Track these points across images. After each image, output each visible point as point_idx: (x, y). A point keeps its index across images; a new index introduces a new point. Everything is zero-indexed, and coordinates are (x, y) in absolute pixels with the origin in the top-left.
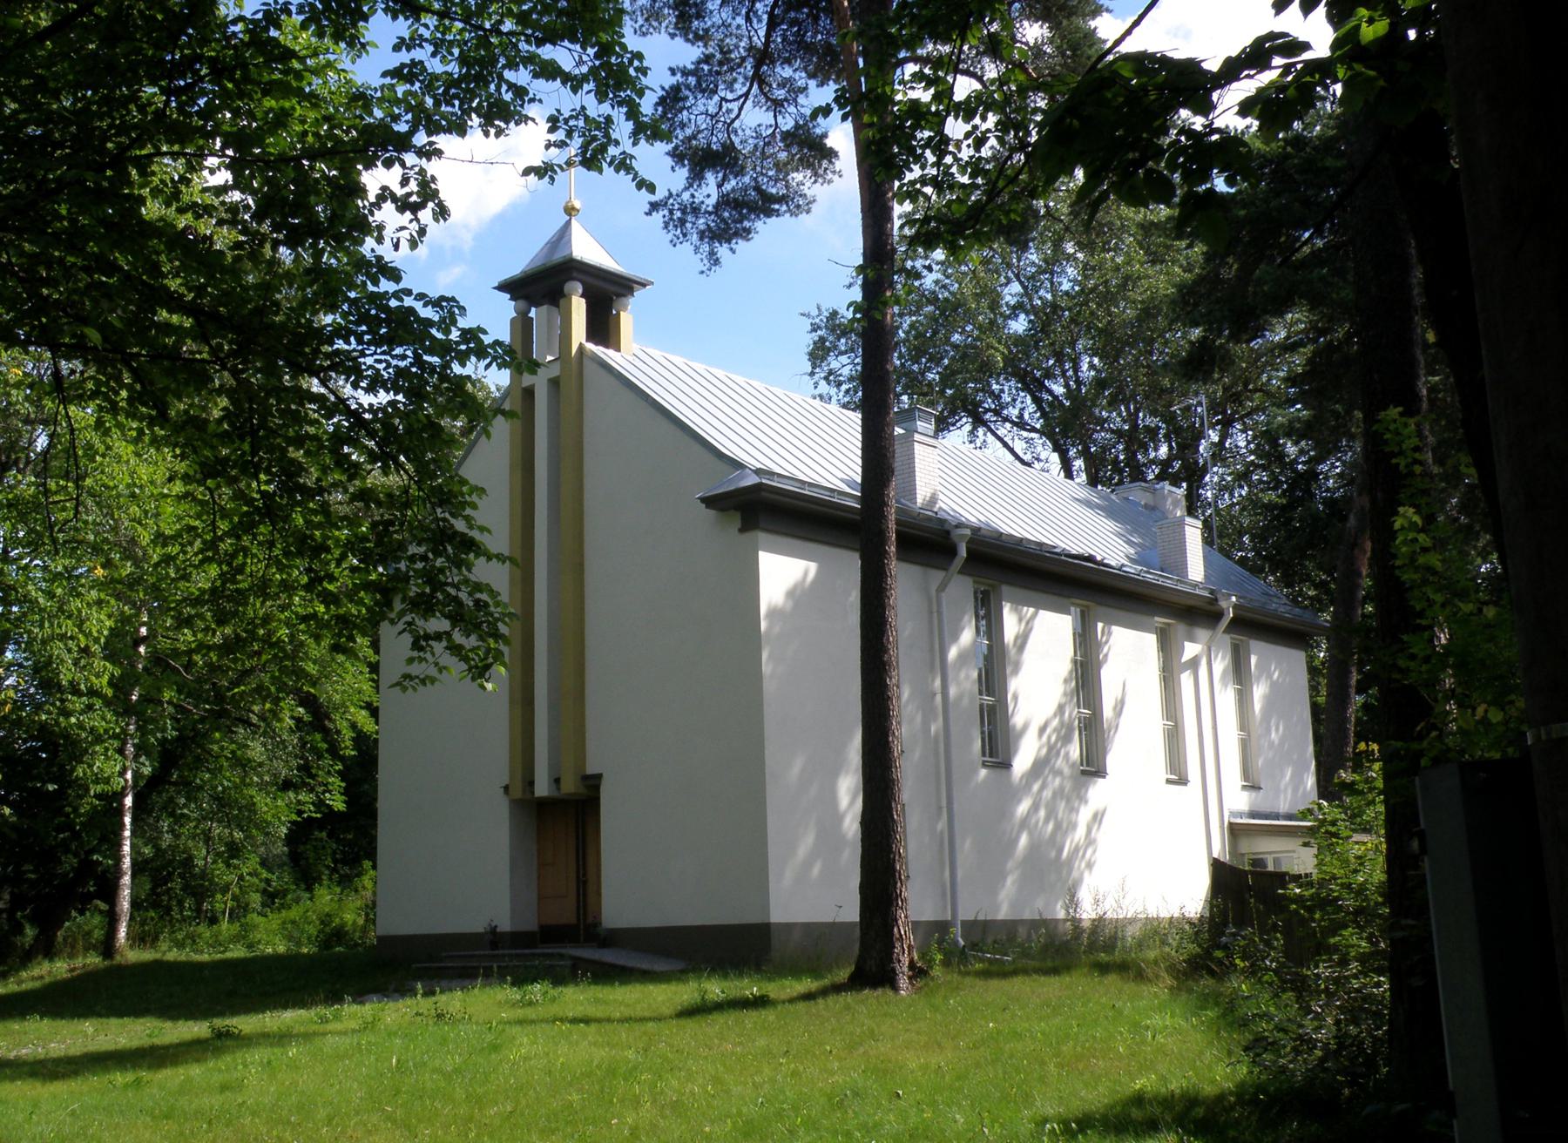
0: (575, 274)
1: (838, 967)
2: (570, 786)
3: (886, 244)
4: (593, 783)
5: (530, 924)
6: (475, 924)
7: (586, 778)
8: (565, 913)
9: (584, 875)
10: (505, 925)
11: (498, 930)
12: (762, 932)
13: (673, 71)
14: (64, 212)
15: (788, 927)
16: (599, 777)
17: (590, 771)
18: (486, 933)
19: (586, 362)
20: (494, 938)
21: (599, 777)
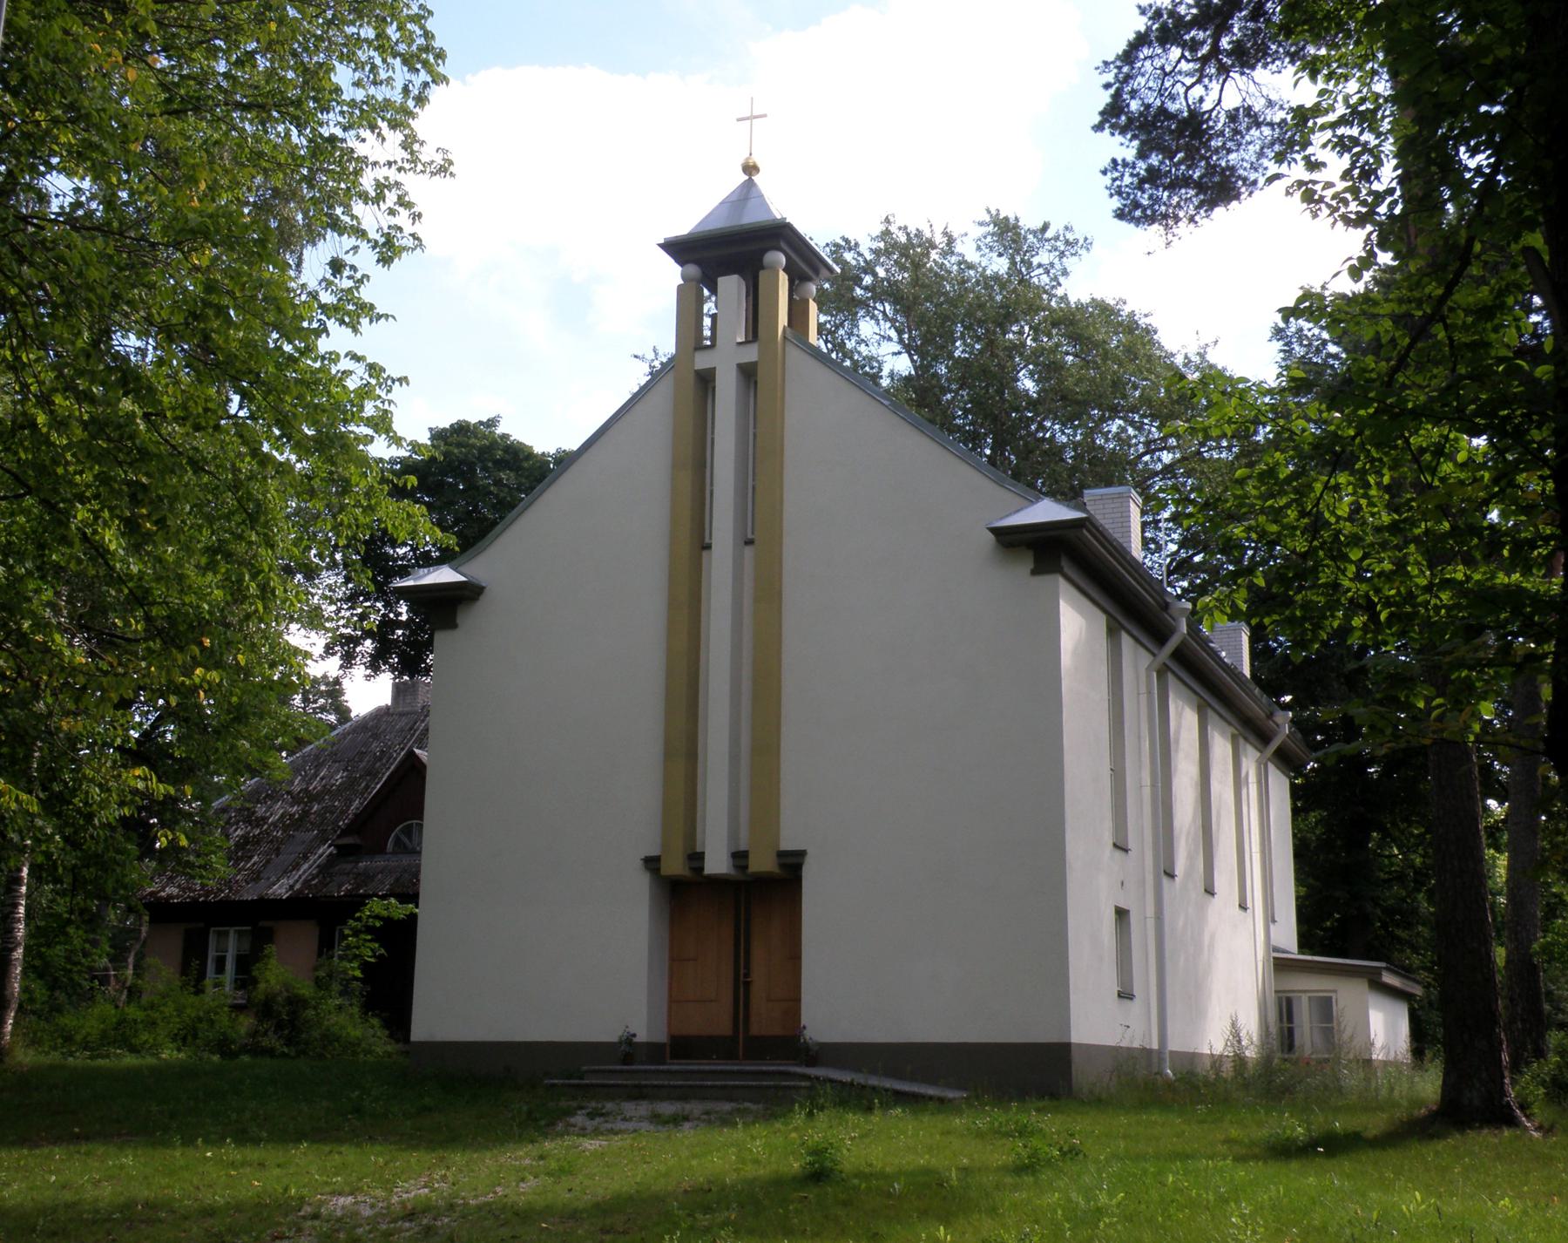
0: (783, 245)
1: (206, 1141)
2: (762, 863)
3: (1386, 281)
4: (792, 865)
5: (661, 1037)
6: (605, 1031)
7: (782, 855)
8: (715, 1020)
9: (747, 975)
10: (642, 1036)
11: (636, 1040)
12: (1062, 1052)
13: (1104, 172)
14: (1396, 852)
15: (1080, 1045)
16: (801, 854)
17: (786, 845)
18: (620, 1043)
19: (1026, 502)
20: (627, 1051)
21: (801, 854)
